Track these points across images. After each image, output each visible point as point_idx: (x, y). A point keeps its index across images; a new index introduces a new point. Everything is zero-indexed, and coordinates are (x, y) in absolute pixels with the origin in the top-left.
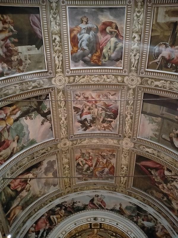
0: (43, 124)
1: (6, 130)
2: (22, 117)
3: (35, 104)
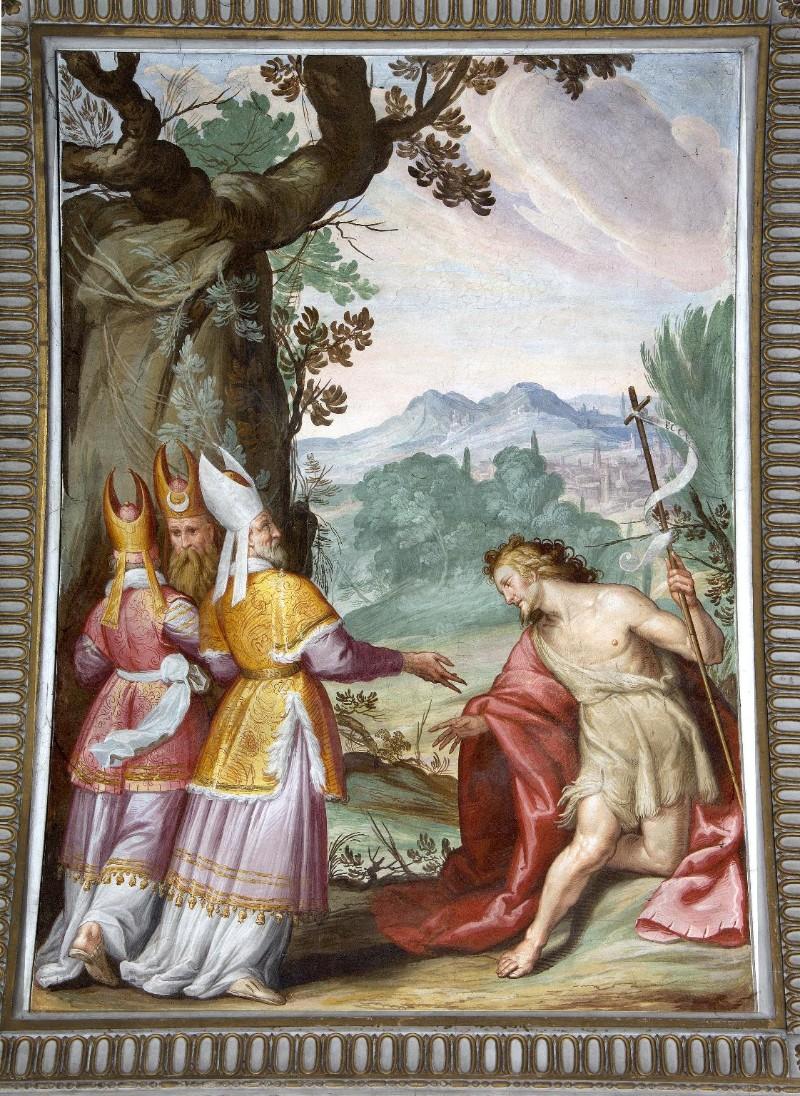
0: (484, 178)
1: (356, 688)
2: (287, 448)
3: (178, 255)
